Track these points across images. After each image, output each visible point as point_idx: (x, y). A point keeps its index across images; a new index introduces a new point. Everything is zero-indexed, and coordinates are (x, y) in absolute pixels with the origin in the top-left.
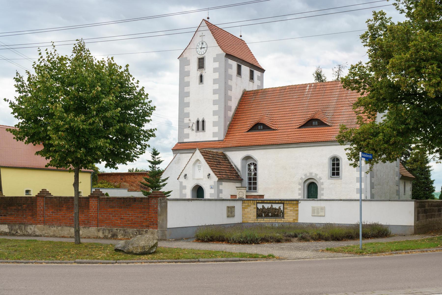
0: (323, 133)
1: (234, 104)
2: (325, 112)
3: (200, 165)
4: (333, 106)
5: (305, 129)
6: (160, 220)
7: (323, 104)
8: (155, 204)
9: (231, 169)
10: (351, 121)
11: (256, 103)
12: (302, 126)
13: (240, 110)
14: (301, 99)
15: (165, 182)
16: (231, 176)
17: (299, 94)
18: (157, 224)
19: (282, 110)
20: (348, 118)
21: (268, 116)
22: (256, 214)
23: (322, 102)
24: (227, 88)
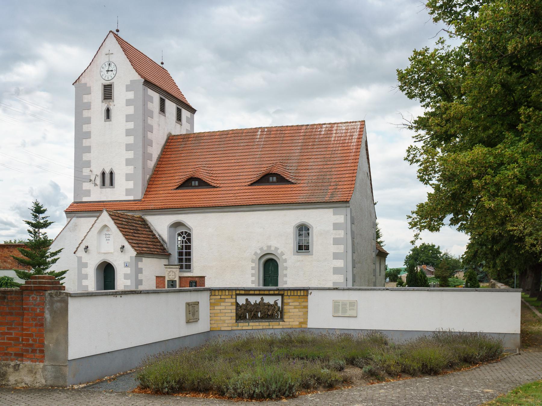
0: (285, 193)
1: (155, 151)
2: (286, 165)
3: (109, 233)
4: (296, 158)
5: (258, 187)
6: (49, 341)
7: (283, 155)
8: (38, 305)
9: (154, 240)
10: (322, 177)
11: (187, 152)
12: (254, 183)
13: (165, 160)
14: (250, 147)
15: (55, 257)
16: (155, 250)
17: (247, 141)
18: (42, 351)
19: (225, 162)
20: (318, 174)
21: (206, 168)
22: (235, 314)
23: (281, 152)
24: (147, 128)
